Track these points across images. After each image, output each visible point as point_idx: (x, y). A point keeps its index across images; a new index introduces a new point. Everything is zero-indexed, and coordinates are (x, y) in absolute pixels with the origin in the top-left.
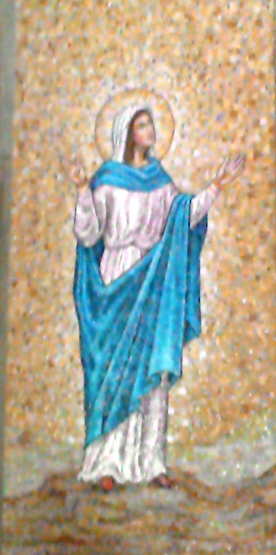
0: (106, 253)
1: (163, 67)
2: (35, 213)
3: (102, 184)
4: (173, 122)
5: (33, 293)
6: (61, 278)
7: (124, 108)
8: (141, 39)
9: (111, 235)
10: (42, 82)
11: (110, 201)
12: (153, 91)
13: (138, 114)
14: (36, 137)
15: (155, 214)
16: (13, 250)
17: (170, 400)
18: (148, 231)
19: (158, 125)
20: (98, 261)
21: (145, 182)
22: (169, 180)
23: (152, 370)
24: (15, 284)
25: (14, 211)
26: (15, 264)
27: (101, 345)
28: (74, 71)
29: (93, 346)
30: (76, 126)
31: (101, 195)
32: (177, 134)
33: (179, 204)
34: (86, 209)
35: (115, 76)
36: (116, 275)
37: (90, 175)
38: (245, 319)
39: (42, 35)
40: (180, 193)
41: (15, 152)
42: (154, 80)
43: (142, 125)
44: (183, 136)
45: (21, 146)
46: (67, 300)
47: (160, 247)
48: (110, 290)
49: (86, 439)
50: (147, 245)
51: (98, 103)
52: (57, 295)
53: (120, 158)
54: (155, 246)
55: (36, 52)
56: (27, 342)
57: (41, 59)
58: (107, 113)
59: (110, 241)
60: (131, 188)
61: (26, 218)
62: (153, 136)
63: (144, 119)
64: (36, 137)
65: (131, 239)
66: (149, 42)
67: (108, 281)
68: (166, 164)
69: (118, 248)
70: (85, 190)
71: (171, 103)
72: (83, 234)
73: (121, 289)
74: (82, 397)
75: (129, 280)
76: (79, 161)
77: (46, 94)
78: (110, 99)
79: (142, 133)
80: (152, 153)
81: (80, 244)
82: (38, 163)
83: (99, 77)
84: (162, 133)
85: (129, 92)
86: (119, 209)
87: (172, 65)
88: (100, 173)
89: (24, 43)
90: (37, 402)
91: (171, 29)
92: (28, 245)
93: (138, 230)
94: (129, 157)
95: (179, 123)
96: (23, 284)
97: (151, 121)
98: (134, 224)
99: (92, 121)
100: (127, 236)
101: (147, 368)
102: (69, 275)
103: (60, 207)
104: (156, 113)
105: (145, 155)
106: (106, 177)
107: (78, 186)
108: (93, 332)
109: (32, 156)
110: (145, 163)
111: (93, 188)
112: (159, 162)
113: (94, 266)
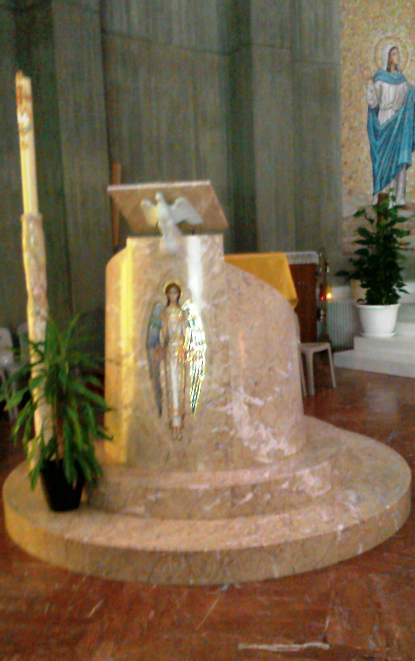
0: (380, 113)
1: (403, 28)
2: (351, 92)
3: (379, 80)
4: (408, 55)
5: (351, 128)
6: (362, 122)
7: (386, 45)
8: (393, 12)
9: (382, 103)
10: (352, 29)
11: (381, 87)
12: (399, 38)
13: (394, 48)
14: (349, 55)
15: (400, 96)
16: (342, 108)
17: (407, 175)
18: (397, 102)
19: (401, 55)
20: (377, 116)
21: (395, 80)
22: (406, 80)
23: (399, 163)
24: (343, 124)
25: (342, 90)
26: (343, 114)
27: (379, 152)
28: (366, 26)
29: (376, 153)
30: (367, 52)
31: (378, 83)
32: (409, 60)
33: (410, 91)
34: (371, 91)
35: (382, 29)
36: (385, 121)
37: (373, 74)
38: (191, 302)
39: (350, 6)
40: (410, 86)
41: (342, 62)
42: (399, 33)
43: (394, 54)
44: (412, 61)
45: (344, 59)
46: (365, 132)
47: (402, 110)
48: (382, 128)
49: (380, 188)
50: (396, 108)
51: (376, 41)
52: (361, 130)
53: (385, 68)
54: (401, 108)
55: (348, 13)
56: (349, 150)
57: (351, 17)
58: (380, 47)
59: (382, 106)
60: (389, 83)
61: (347, 94)
62: (399, 59)
63: (395, 51)
64: (349, 55)
65: (390, 106)
66: (397, 14)
67: (381, 124)
68: (404, 73)
69: (385, 109)
70: (370, 82)
71: (407, 45)
72: (371, 102)
73: (386, 127)
74: (372, 174)
75: (390, 124)
76: (368, 68)
77: (353, 35)
78: (381, 40)
79: (395, 58)
80: (398, 68)
81: (369, 107)
82: (351, 68)
83: (376, 29)
84: (403, 59)
85: (388, 38)
86: (385, 91)
87: (407, 27)
88: (377, 75)
89: (344, 8)
90: (354, 176)
91: (406, 11)
92: (348, 106)
93: (393, 102)
94: (389, 70)
95: (410, 55)
96: (347, 125)
97: (398, 53)
98: (391, 98)
99: (373, 50)
100: (388, 105)
101: (397, 162)
102: (365, 121)
103: (361, 90)
104: (400, 49)
105: (396, 68)
106: (381, 77)
107: (368, 80)
108: (376, 147)
109: (348, 64)
110: (395, 72)
111: (374, 81)
112: (401, 71)
113: (375, 117)
